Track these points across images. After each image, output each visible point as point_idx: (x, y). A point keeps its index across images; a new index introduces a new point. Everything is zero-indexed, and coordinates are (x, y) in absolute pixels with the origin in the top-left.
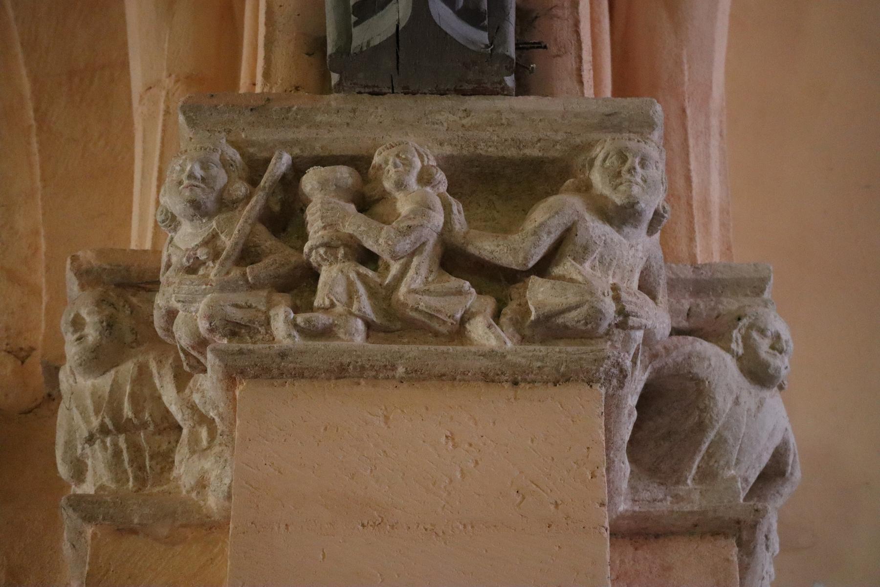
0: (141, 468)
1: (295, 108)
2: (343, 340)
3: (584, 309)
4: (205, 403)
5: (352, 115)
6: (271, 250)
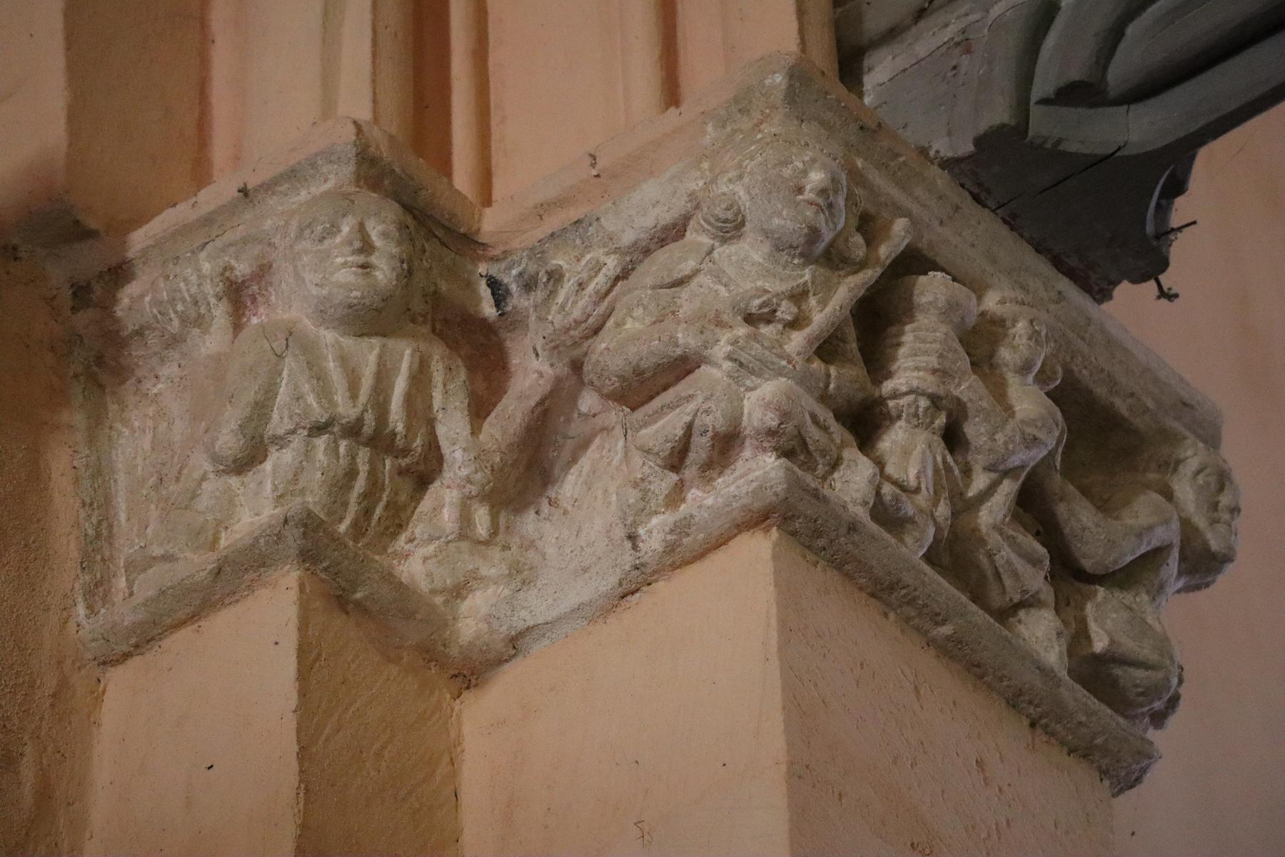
0: (368, 513)
1: (902, 159)
3: (1157, 676)
4: (643, 510)
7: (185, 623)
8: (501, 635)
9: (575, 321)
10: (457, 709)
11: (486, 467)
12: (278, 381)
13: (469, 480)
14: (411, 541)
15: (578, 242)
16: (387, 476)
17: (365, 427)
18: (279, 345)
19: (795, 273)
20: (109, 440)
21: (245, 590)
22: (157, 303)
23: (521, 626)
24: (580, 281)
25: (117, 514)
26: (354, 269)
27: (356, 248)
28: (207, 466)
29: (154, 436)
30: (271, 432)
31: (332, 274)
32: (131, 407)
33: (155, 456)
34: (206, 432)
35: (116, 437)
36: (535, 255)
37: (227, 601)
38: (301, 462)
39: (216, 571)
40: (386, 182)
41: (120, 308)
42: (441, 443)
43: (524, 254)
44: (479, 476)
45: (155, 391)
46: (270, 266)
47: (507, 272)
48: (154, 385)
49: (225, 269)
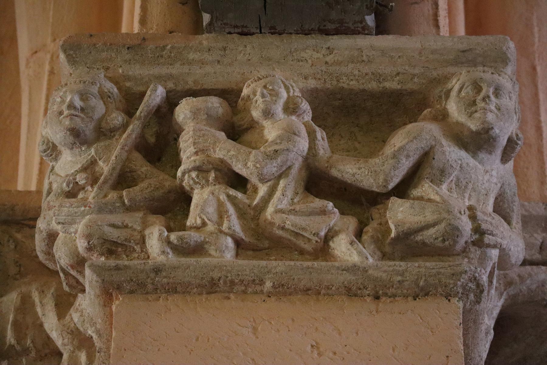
1: (169, 47)
2: (214, 257)
5: (222, 53)
6: (146, 175)
19: (86, 155)
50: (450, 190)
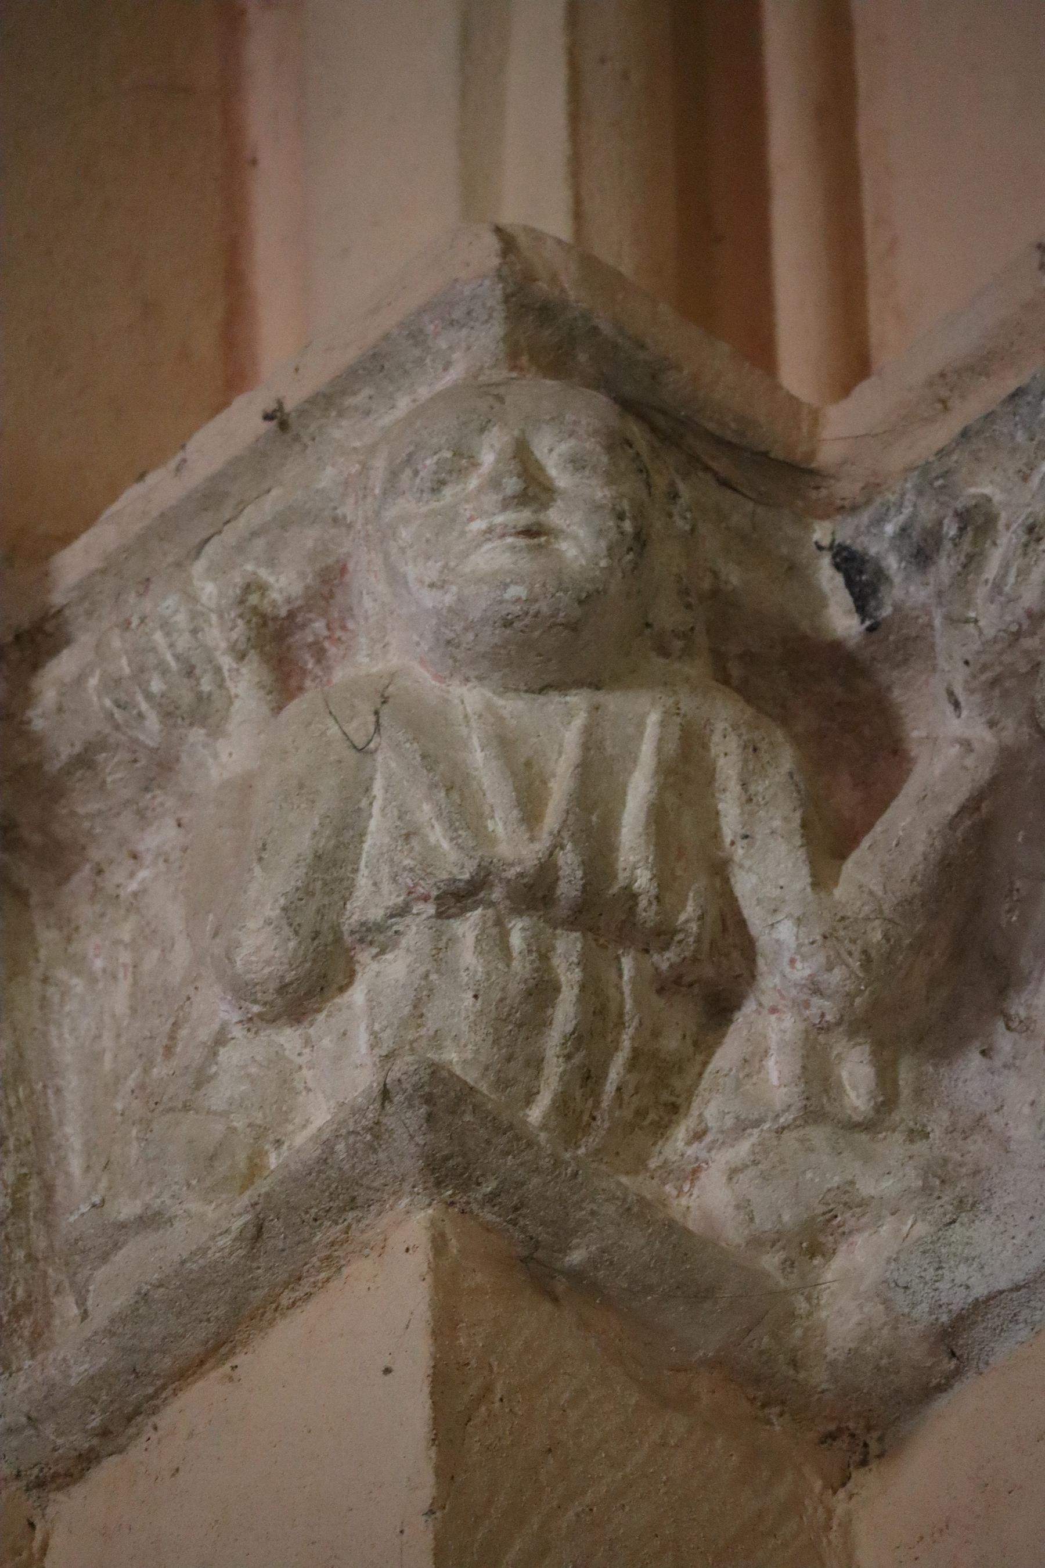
7: (202, 1363)
8: (918, 1327)
9: (1030, 614)
10: (840, 1510)
11: (850, 954)
12: (364, 803)
13: (816, 989)
14: (698, 1136)
15: (1020, 436)
16: (627, 989)
17: (560, 883)
18: (359, 727)
20: (42, 1007)
21: (319, 1271)
22: (112, 684)
23: (959, 1300)
24: (1030, 520)
25: (62, 1161)
26: (510, 540)
27: (509, 492)
28: (227, 1012)
29: (135, 983)
30: (355, 917)
31: (465, 555)
32: (84, 930)
33: (137, 1025)
34: (215, 935)
35: (56, 999)
36: (931, 484)
37: (285, 1301)
38: (426, 976)
39: (251, 1231)
40: (582, 357)
41: (39, 711)
42: (746, 913)
43: (909, 485)
44: (837, 976)
45: (133, 886)
46: (343, 570)
47: (874, 531)
48: (132, 875)
49: (247, 589)
50: (302, 858)
